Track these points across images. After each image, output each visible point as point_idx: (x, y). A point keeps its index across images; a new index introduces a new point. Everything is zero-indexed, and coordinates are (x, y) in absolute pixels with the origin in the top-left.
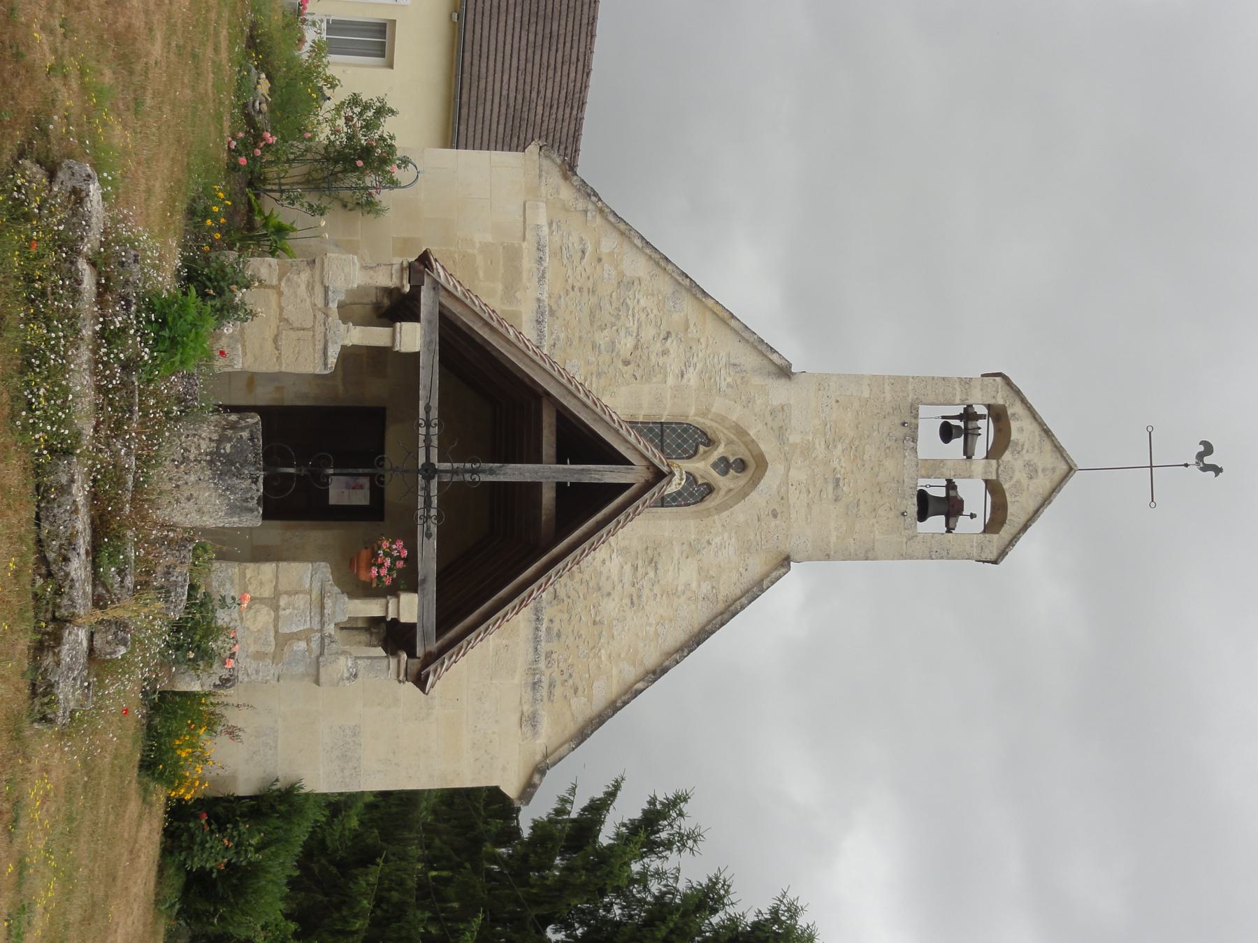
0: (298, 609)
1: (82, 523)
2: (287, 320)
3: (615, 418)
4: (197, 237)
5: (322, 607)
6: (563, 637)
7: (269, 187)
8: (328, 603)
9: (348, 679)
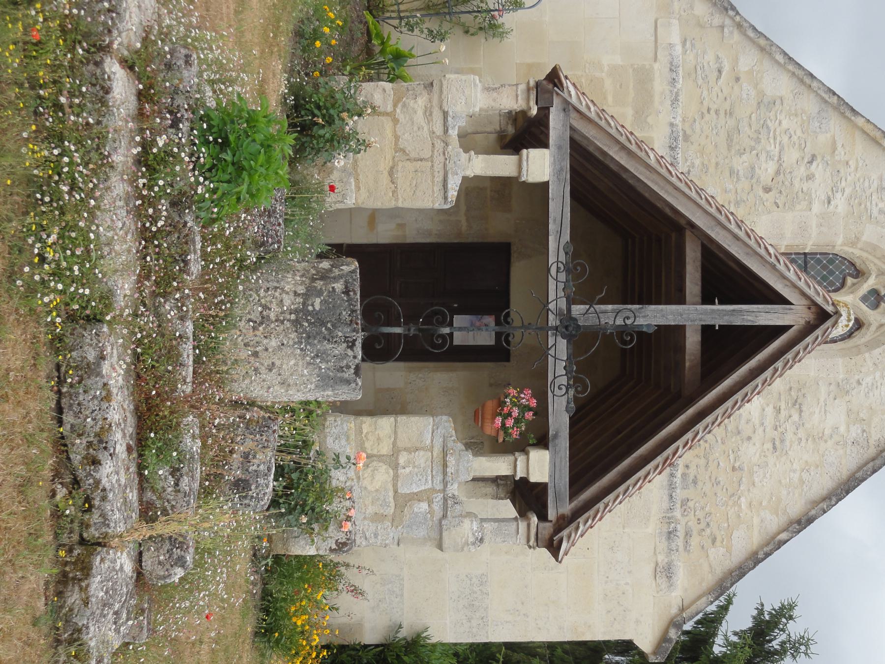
0: (419, 467)
1: (119, 413)
2: (403, 151)
3: (772, 251)
4: (307, 64)
5: (445, 466)
6: (700, 484)
7: (388, 15)
8: (451, 460)
9: (474, 544)
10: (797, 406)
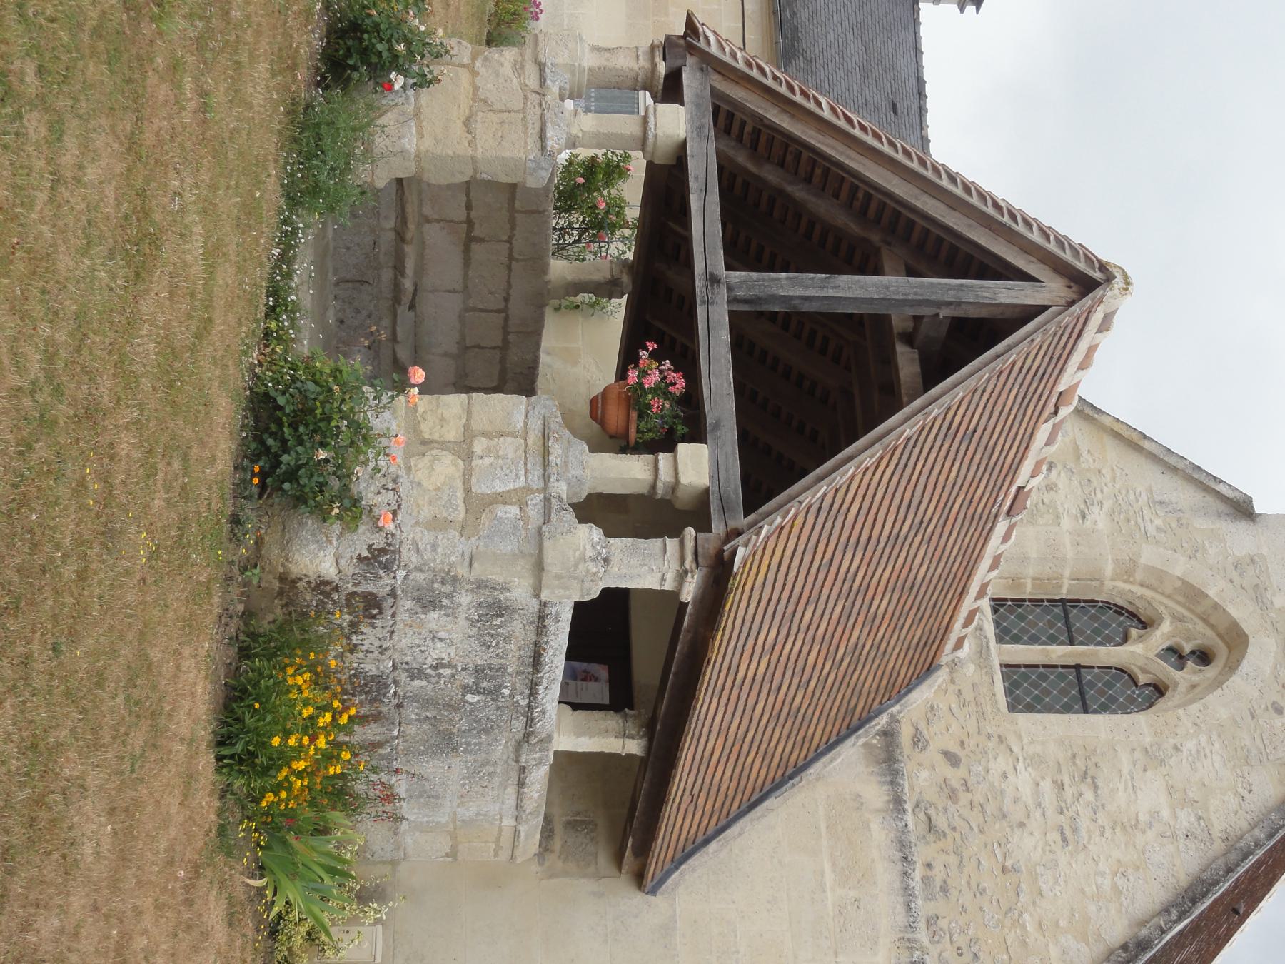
2: (485, 101)
5: (546, 452)
8: (556, 451)
10: (1089, 780)
